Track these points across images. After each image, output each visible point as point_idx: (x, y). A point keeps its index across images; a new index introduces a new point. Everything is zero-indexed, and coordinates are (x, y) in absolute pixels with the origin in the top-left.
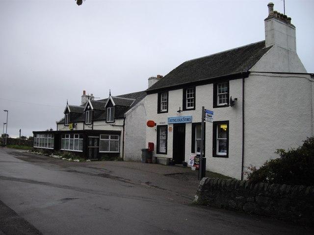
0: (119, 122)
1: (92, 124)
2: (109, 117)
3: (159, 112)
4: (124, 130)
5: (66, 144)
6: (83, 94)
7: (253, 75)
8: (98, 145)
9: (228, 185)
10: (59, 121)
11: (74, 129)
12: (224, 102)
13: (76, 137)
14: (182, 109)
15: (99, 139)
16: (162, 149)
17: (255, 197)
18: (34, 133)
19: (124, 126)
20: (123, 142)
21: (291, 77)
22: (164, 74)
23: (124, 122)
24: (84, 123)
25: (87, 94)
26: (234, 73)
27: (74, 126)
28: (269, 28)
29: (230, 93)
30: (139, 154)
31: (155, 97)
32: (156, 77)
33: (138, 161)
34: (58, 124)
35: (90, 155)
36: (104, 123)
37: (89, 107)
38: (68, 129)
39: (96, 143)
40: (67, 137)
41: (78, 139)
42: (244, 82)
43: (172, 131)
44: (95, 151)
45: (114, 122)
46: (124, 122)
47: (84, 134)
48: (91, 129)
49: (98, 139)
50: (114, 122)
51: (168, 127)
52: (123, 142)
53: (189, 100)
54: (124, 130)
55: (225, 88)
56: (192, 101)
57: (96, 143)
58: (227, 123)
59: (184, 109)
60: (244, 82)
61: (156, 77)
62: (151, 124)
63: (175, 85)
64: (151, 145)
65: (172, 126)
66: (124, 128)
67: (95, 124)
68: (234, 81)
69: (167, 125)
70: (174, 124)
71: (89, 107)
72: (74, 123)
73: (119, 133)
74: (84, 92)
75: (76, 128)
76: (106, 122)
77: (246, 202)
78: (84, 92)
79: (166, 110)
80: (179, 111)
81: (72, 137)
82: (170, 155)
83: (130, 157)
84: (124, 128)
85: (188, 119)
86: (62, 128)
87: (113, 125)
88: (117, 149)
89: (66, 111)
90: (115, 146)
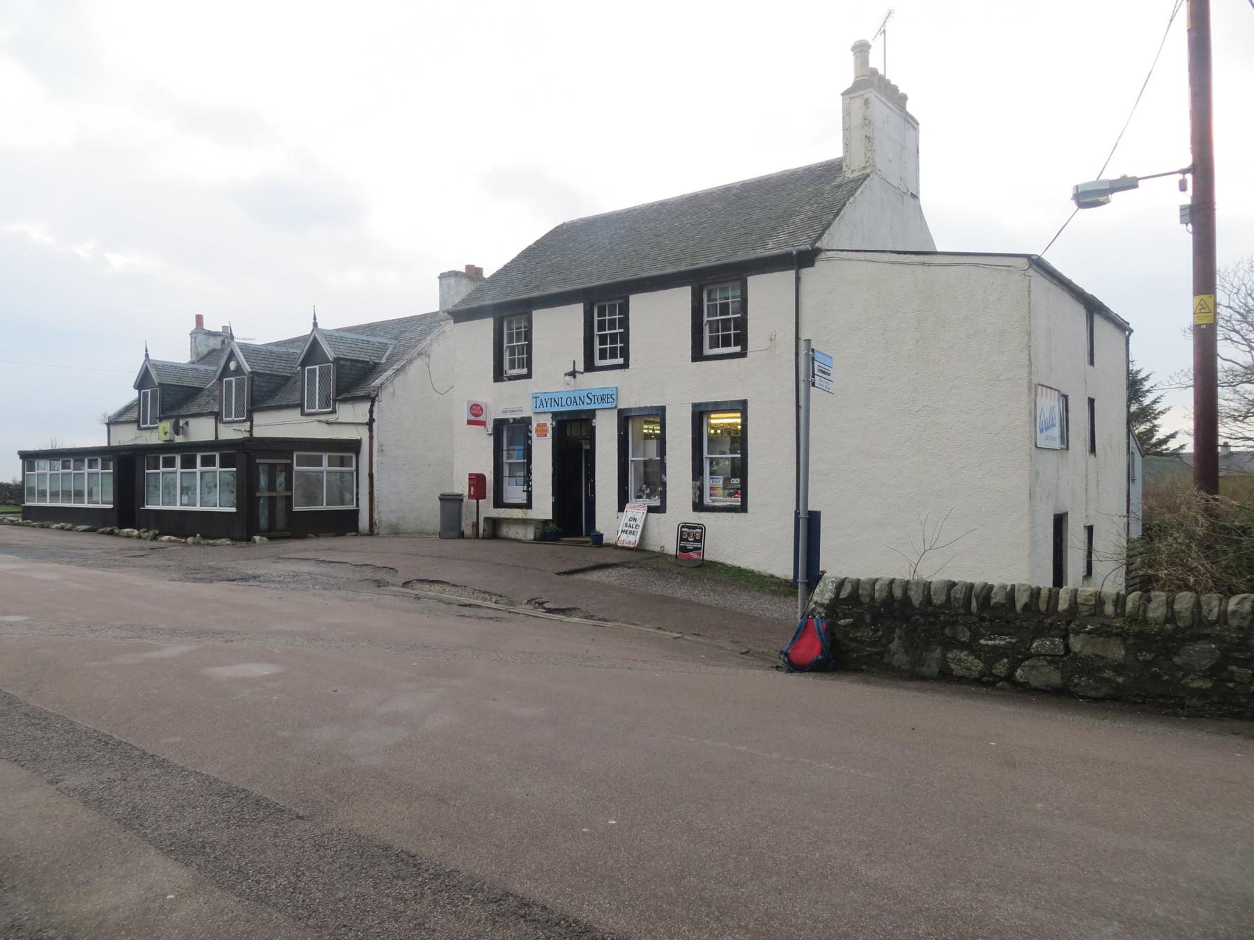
0: (351, 413)
1: (250, 419)
2: (312, 394)
3: (499, 376)
4: (371, 438)
5: (166, 487)
6: (194, 326)
7: (829, 259)
8: (289, 486)
9: (939, 599)
10: (114, 408)
11: (179, 439)
12: (614, 356)
13: (208, 461)
14: (580, 366)
15: (291, 465)
16: (514, 493)
17: (1065, 638)
18: (29, 458)
19: (370, 424)
20: (371, 476)
21: (957, 264)
22: (1129, 176)
23: (371, 412)
24: (217, 416)
25: (208, 326)
26: (762, 253)
27: (177, 430)
28: (857, 120)
29: (749, 316)
30: (432, 516)
31: (485, 329)
32: (464, 270)
33: (421, 534)
34: (112, 422)
35: (263, 522)
36: (295, 414)
37: (232, 366)
38: (154, 438)
39: (281, 479)
40: (169, 463)
41: (217, 468)
42: (798, 279)
43: (549, 435)
44: (281, 505)
45: (334, 411)
46: (371, 412)
47: (230, 452)
48: (247, 435)
49: (288, 469)
50: (334, 411)
51: (534, 425)
52: (371, 476)
53: (603, 340)
54: (371, 438)
55: (733, 302)
56: (614, 340)
57: (281, 479)
58: (741, 407)
59: (590, 366)
60: (798, 279)
61: (464, 270)
62: (476, 415)
63: (555, 290)
64: (477, 481)
65: (548, 422)
66: (371, 430)
67: (259, 418)
68: (635, 295)
69: (530, 418)
70: (555, 415)
71: (232, 366)
72: (178, 418)
73: (354, 446)
74: (199, 319)
75: (185, 434)
76: (303, 414)
77: (1029, 657)
78: (199, 319)
79: (525, 371)
80: (573, 374)
81: (189, 463)
82: (543, 508)
83: (394, 521)
84: (371, 430)
85: (604, 398)
86: (127, 436)
87: (328, 423)
88: (347, 496)
89: (143, 382)
90: (344, 487)
